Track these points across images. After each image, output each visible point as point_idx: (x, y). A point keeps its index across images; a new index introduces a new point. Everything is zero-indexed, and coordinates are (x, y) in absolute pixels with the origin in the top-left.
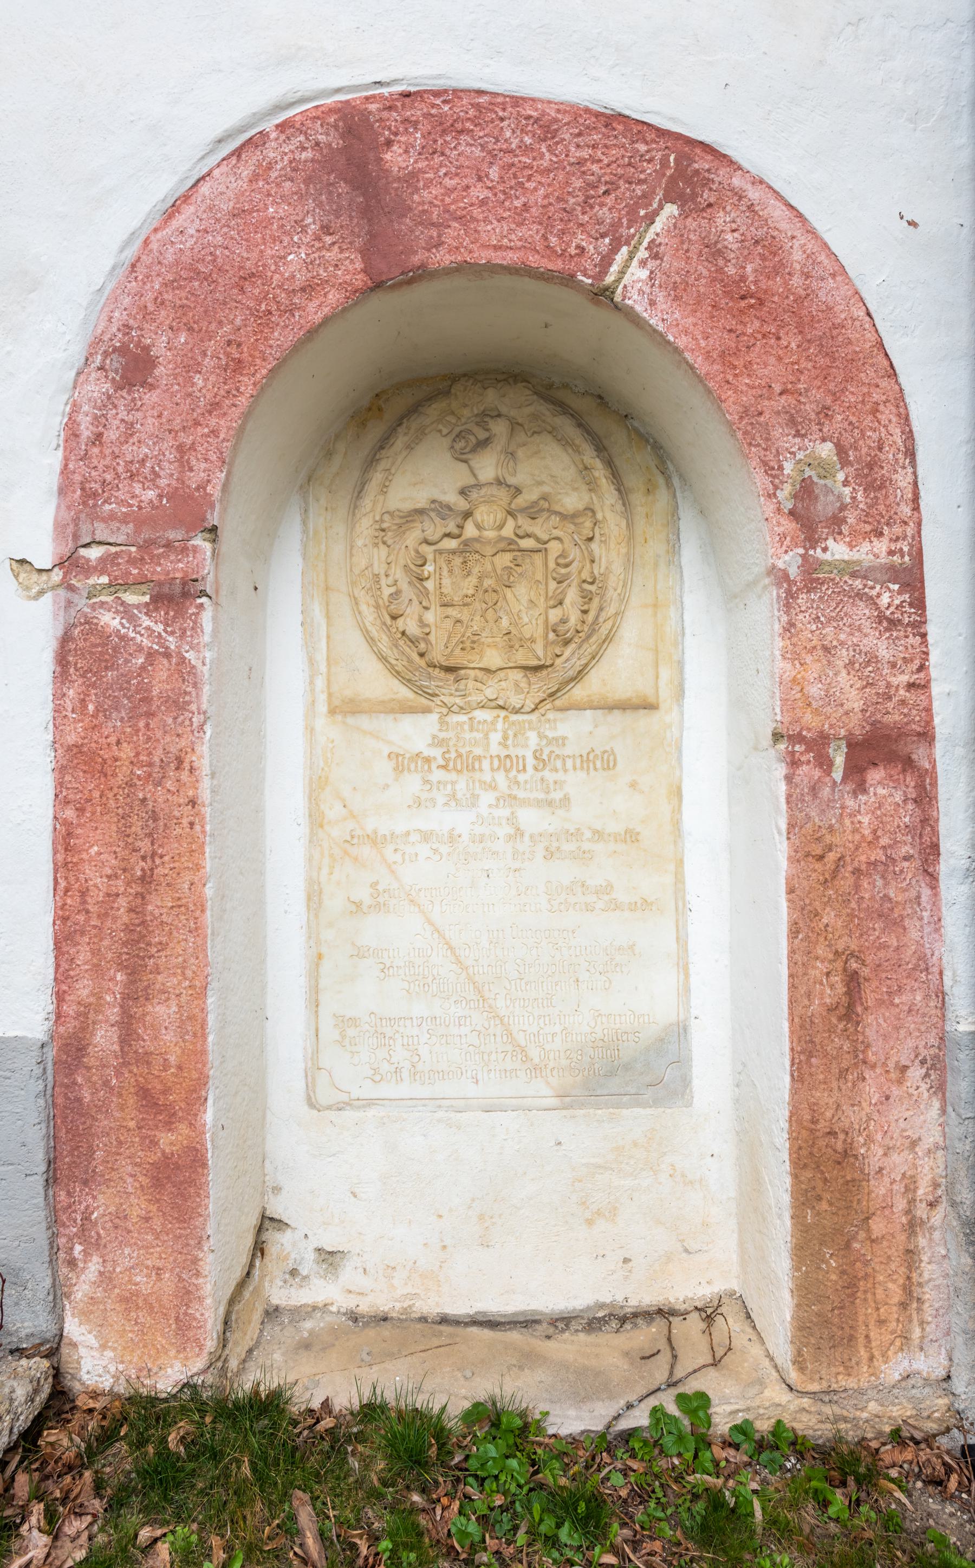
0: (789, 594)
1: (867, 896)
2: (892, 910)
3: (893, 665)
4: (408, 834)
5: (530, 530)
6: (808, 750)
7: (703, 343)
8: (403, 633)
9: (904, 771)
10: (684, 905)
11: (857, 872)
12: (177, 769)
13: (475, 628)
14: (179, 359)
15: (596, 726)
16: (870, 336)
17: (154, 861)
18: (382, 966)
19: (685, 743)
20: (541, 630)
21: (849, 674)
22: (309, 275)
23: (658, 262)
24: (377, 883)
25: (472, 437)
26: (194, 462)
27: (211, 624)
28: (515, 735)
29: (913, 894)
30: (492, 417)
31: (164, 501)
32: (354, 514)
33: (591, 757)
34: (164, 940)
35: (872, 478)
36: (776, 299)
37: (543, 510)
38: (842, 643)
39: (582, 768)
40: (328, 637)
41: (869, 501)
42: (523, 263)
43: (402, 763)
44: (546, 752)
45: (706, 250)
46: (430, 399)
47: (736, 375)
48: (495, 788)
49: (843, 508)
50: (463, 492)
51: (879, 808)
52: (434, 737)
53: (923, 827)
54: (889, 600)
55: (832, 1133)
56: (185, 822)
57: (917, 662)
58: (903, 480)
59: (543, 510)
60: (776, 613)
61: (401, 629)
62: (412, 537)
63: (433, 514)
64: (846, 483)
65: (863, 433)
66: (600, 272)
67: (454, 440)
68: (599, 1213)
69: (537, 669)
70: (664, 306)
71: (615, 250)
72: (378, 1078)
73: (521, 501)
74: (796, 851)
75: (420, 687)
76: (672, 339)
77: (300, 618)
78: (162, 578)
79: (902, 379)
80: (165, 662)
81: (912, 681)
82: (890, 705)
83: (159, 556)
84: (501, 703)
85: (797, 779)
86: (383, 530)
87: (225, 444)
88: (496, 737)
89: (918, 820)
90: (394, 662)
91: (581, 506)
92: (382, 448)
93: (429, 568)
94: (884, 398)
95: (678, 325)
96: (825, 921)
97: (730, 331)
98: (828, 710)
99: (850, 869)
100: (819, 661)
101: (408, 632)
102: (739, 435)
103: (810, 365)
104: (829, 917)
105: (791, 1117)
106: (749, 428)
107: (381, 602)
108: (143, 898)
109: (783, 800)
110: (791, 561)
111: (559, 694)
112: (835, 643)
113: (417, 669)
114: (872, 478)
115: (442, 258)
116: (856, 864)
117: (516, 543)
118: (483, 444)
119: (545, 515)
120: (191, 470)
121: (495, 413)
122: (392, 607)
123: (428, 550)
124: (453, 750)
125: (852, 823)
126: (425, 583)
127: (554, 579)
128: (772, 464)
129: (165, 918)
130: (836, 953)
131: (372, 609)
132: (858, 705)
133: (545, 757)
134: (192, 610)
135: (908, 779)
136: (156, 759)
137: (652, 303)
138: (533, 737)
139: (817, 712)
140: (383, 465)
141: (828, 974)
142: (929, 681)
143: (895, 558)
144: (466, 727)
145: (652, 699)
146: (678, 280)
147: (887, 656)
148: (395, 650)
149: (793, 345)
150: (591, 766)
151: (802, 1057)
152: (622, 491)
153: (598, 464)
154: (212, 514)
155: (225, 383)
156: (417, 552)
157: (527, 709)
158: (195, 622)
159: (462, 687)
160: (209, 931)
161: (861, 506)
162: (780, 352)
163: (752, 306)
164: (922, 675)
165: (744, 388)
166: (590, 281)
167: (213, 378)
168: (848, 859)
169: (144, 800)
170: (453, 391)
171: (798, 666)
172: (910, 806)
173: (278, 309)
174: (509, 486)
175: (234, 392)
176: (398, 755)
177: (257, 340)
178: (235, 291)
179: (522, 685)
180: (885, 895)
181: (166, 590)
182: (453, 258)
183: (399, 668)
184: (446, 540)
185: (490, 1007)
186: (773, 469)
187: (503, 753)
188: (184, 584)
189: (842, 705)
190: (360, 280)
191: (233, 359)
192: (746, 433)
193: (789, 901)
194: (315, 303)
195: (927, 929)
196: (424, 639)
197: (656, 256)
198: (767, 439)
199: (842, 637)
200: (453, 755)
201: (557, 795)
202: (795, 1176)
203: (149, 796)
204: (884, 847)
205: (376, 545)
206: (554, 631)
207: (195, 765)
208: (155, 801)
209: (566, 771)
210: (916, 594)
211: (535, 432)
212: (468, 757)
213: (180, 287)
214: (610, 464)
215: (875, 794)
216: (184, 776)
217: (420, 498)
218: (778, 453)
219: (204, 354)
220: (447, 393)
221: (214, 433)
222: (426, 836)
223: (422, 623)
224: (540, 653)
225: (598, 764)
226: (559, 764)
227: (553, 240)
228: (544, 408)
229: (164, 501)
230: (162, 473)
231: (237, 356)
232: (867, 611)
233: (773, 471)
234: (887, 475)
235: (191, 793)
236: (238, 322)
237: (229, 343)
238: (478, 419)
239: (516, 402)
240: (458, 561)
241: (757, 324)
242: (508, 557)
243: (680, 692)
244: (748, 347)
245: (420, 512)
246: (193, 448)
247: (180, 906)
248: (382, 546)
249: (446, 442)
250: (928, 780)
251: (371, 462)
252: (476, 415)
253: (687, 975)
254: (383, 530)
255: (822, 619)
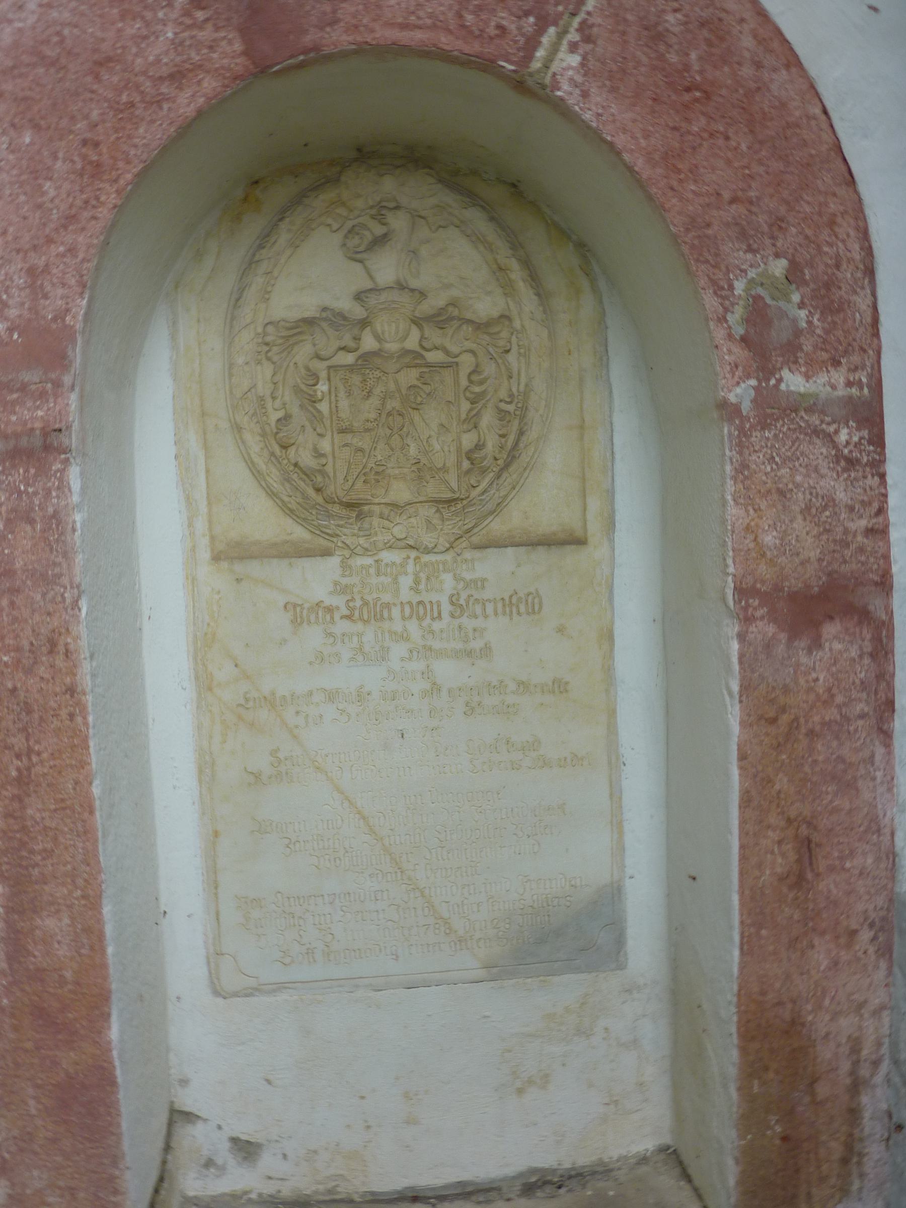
0: (743, 433)
1: (821, 758)
2: (845, 771)
3: (851, 509)
4: (310, 693)
5: (438, 341)
6: (761, 605)
7: (643, 143)
8: (296, 465)
9: (860, 623)
10: (618, 759)
11: (811, 733)
12: (51, 652)
13: (379, 458)
14: (24, 163)
15: (519, 566)
16: (826, 136)
17: (30, 759)
18: (287, 841)
19: (616, 581)
20: (452, 460)
21: (805, 519)
22: (178, 59)
23: (591, 46)
24: (277, 750)
25: (367, 233)
26: (48, 288)
27: (79, 480)
28: (428, 579)
29: (866, 753)
30: (391, 209)
31: (15, 336)
32: (231, 327)
33: (514, 600)
34: (49, 846)
35: (828, 300)
36: (724, 92)
37: (452, 318)
38: (798, 486)
39: (504, 613)
40: (207, 471)
41: (826, 325)
42: (435, 45)
43: (300, 614)
44: (464, 596)
45: (645, 33)
46: (316, 188)
47: (681, 181)
48: (408, 639)
49: (798, 333)
50: (359, 297)
51: (835, 664)
52: (336, 584)
53: (878, 682)
54: (847, 437)
55: (780, 1004)
56: (64, 713)
57: (876, 505)
58: (862, 302)
59: (452, 318)
60: (728, 453)
61: (293, 461)
62: (303, 353)
63: (324, 325)
64: (801, 305)
65: (819, 248)
66: (524, 57)
67: (346, 237)
68: (530, 1082)
69: (450, 502)
70: (599, 99)
71: (541, 30)
72: (287, 960)
73: (426, 308)
74: (749, 715)
75: (318, 527)
76: (609, 138)
77: (173, 450)
78: (19, 429)
79: (862, 188)
80: (28, 528)
81: (870, 526)
82: (847, 553)
83: (14, 403)
84: (411, 543)
85: (751, 637)
86: (267, 344)
87: (86, 265)
88: (406, 582)
89: (873, 675)
90: (286, 499)
91: (495, 314)
92: (261, 247)
93: (323, 387)
94: (841, 208)
95: (614, 121)
96: (777, 787)
97: (675, 128)
98: (782, 560)
99: (803, 730)
100: (774, 506)
101: (302, 465)
102: (685, 249)
103: (761, 170)
104: (782, 782)
105: (739, 991)
106: (696, 242)
107: (267, 428)
108: (21, 800)
109: (735, 660)
110: (742, 393)
111: (476, 530)
112: (790, 486)
113: (313, 507)
114: (828, 300)
115: (338, 38)
116: (810, 725)
117: (422, 356)
118: (380, 241)
119: (455, 323)
120: (46, 297)
121: (392, 205)
122: (281, 435)
123: (320, 367)
124: (357, 597)
125: (807, 681)
126: (317, 405)
127: (467, 399)
128: (721, 283)
129: (48, 823)
130: (789, 821)
131: (258, 438)
132: (814, 554)
133: (462, 602)
134: (57, 466)
135: (865, 631)
136: (25, 644)
137: (585, 95)
138: (448, 579)
139: (772, 563)
140: (264, 267)
141: (780, 842)
142: (887, 526)
143: (854, 390)
144: (372, 571)
145: (579, 533)
146: (615, 68)
147: (845, 499)
148: (287, 485)
149: (744, 147)
150: (514, 610)
151: (752, 930)
152: (543, 296)
153: (514, 264)
154: (74, 350)
155: (82, 191)
156: (308, 369)
157: (440, 548)
158: (61, 480)
159: (366, 526)
160: (100, 834)
161: (818, 331)
162: (730, 155)
163: (697, 100)
164: (881, 519)
165: (690, 196)
166: (512, 68)
167: (66, 186)
168: (802, 720)
169: (14, 690)
170: (343, 178)
171: (751, 512)
172: (867, 661)
173: (143, 101)
174: (412, 290)
175: (94, 202)
176: (295, 606)
177: (118, 138)
178: (89, 79)
179: (435, 521)
180: (838, 757)
181: (24, 442)
182: (351, 38)
183: (293, 506)
184: (341, 353)
185: (409, 879)
186: (723, 288)
187: (415, 599)
188: (45, 434)
189: (798, 554)
190: (240, 64)
191: (91, 163)
192: (693, 247)
193: (741, 768)
194: (188, 93)
195: (881, 790)
196: (319, 471)
197: (588, 39)
198: (717, 255)
199: (799, 478)
200: (358, 603)
201: (477, 644)
202: (743, 1050)
203: (19, 685)
204: (839, 707)
205: (259, 363)
206: (468, 458)
207: (72, 647)
208: (27, 691)
209: (486, 617)
210: (875, 430)
211: (441, 226)
212: (375, 605)
213: (21, 75)
214: (526, 263)
215: (831, 649)
216: (60, 662)
217: (308, 304)
218: (728, 271)
219: (56, 158)
220: (335, 181)
221: (72, 250)
222: (331, 696)
223: (318, 454)
224: (454, 485)
225: (522, 608)
226: (478, 609)
227: (469, 18)
228: (449, 198)
229: (15, 336)
230: (11, 302)
231: (95, 158)
232: (824, 450)
233: (722, 290)
234: (846, 297)
235: (68, 680)
236: (95, 115)
237: (85, 142)
238: (374, 212)
239: (418, 192)
240: (356, 379)
241: (703, 121)
242: (414, 373)
243: (610, 525)
244: (694, 148)
245: (310, 322)
246: (46, 269)
247: (64, 809)
248: (265, 363)
249: (338, 238)
250: (884, 633)
251: (250, 264)
252: (372, 207)
253: (621, 833)
254: (267, 344)
255: (777, 459)
